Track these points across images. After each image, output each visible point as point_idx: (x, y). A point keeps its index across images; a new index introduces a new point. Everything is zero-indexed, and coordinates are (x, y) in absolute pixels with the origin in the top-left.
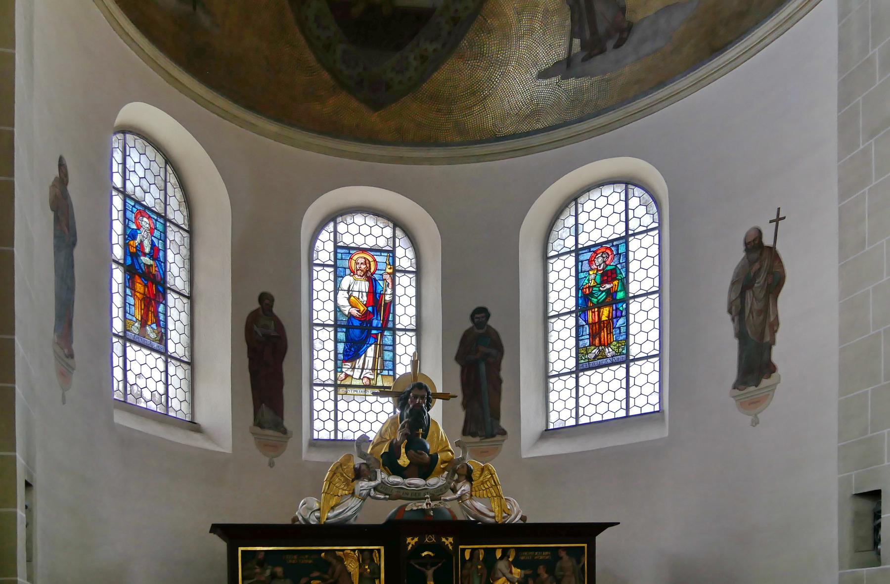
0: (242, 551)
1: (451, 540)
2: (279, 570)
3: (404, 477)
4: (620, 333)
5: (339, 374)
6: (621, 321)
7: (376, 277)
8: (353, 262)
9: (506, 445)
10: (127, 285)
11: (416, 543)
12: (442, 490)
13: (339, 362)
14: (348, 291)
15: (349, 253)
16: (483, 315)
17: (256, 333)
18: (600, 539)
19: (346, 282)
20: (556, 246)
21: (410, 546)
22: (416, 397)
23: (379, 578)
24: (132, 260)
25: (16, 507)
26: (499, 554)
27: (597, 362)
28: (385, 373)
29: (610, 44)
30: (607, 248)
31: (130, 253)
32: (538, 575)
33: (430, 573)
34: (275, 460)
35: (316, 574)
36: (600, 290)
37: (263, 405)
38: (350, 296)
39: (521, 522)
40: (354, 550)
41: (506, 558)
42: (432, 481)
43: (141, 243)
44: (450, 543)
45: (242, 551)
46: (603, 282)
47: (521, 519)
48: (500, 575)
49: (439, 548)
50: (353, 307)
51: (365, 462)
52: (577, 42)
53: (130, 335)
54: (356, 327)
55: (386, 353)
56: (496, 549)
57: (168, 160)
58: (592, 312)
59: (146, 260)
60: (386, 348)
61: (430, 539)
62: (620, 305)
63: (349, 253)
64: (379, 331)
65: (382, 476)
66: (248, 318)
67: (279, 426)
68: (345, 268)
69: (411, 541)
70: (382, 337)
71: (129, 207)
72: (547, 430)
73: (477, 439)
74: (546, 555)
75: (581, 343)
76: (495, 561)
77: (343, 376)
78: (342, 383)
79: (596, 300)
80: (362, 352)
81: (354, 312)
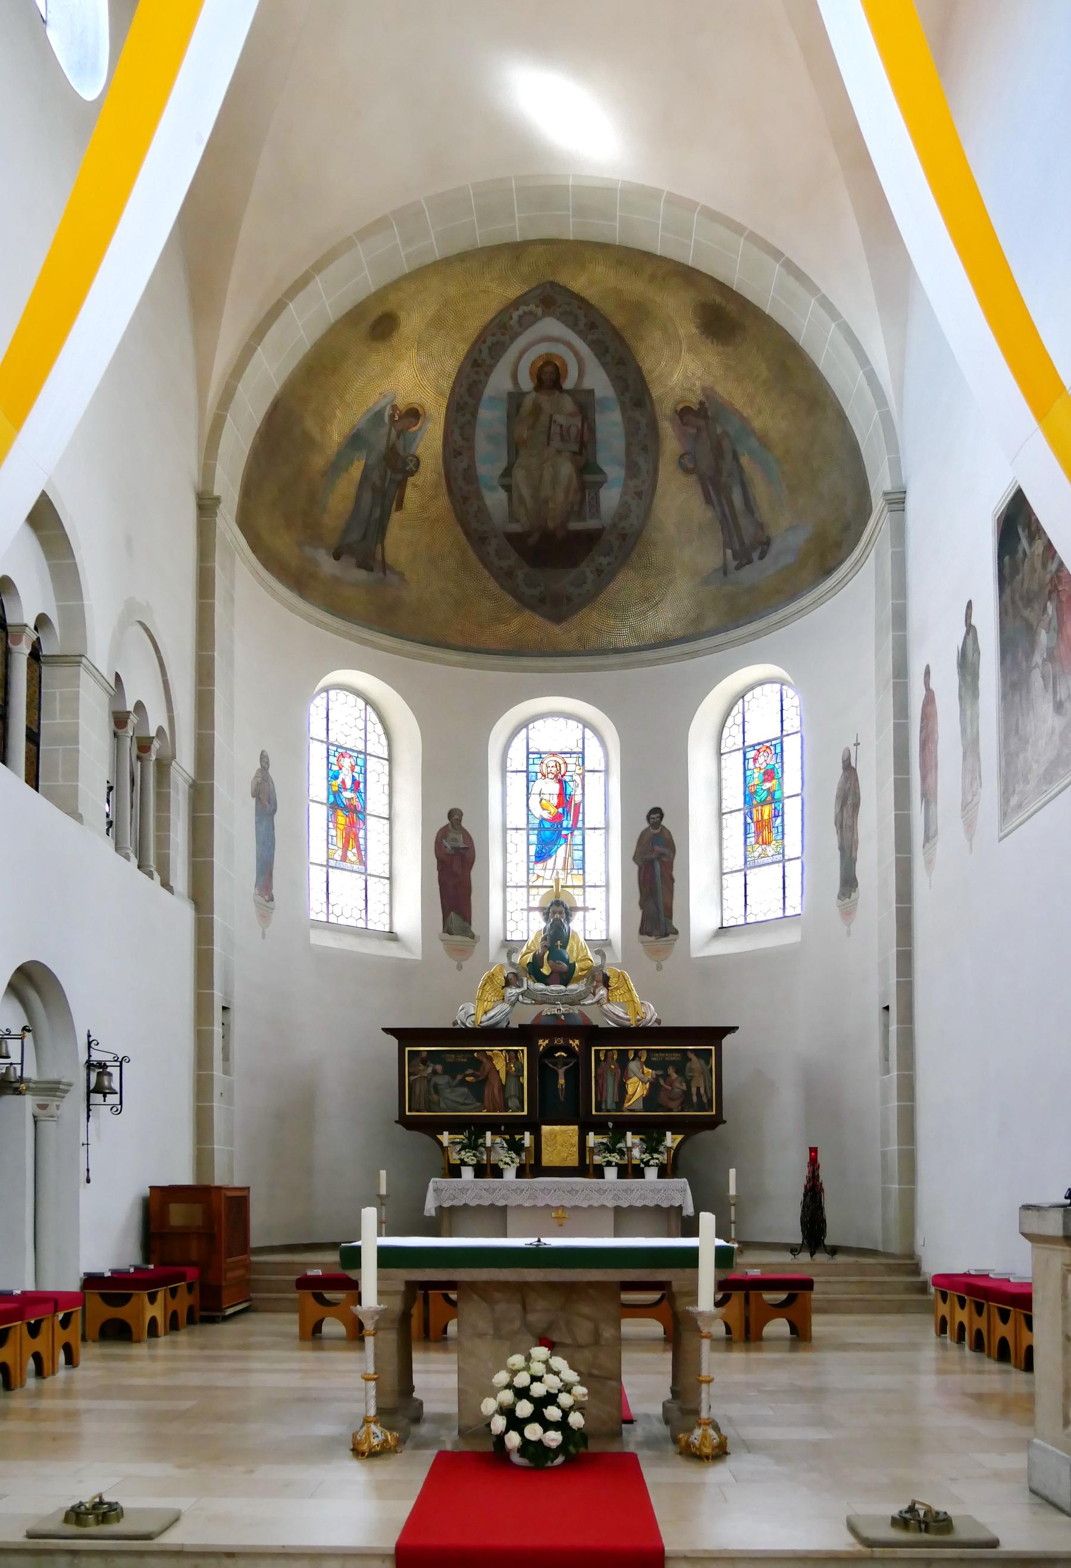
0: (409, 1051)
1: (577, 1042)
2: (439, 1068)
3: (547, 984)
4: (778, 832)
5: (530, 875)
6: (779, 820)
7: (567, 778)
8: (544, 766)
9: (679, 943)
10: (330, 820)
11: (547, 1044)
12: (583, 996)
14: (540, 794)
15: (541, 758)
16: (658, 815)
17: (446, 847)
18: (727, 1041)
19: (536, 788)
20: (728, 744)
21: (542, 1047)
22: (554, 913)
23: (523, 1076)
24: (335, 797)
25: (213, 1025)
28: (575, 872)
29: (755, 555)
30: (767, 747)
31: (333, 791)
32: (669, 1076)
33: (561, 1072)
34: (463, 963)
35: (470, 1071)
36: (762, 789)
38: (541, 800)
39: (656, 1025)
40: (501, 1051)
41: (637, 1058)
42: (571, 987)
43: (343, 782)
45: (409, 1051)
46: (764, 781)
48: (633, 1075)
49: (567, 1049)
50: (544, 809)
51: (514, 971)
52: (729, 552)
53: (332, 863)
54: (547, 829)
55: (576, 853)
57: (368, 702)
58: (757, 810)
59: (348, 794)
60: (576, 847)
61: (559, 1041)
62: (778, 804)
63: (541, 758)
64: (570, 832)
65: (528, 983)
66: (438, 833)
67: (466, 930)
68: (537, 773)
69: (543, 1043)
70: (572, 837)
71: (331, 752)
73: (653, 938)
74: (676, 1057)
75: (748, 840)
76: (628, 1061)
77: (535, 877)
78: (534, 884)
79: (759, 798)
81: (546, 815)
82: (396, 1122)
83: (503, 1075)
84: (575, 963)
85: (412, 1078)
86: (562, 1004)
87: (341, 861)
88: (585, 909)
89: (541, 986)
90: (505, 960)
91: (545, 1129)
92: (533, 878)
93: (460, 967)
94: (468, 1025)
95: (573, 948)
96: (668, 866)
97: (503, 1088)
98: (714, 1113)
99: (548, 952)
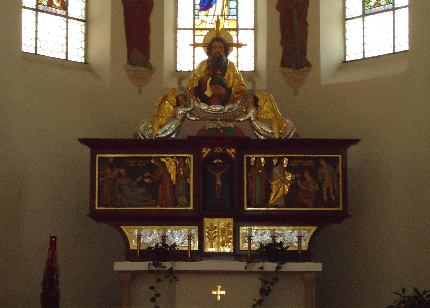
1: (233, 150)
3: (209, 104)
11: (209, 152)
13: (196, 12)
18: (352, 151)
21: (205, 155)
23: (189, 178)
26: (275, 162)
27: (376, 9)
28: (230, 18)
32: (305, 178)
33: (218, 175)
35: (147, 174)
37: (135, 48)
39: (295, 137)
40: (172, 158)
41: (280, 164)
44: (233, 153)
47: (294, 135)
49: (225, 156)
53: (41, 7)
56: (273, 157)
61: (219, 150)
65: (195, 103)
69: (206, 151)
72: (345, 62)
73: (291, 70)
80: (213, 2)
82: (88, 215)
83: (173, 177)
84: (231, 88)
85: (102, 179)
86: (221, 120)
87: (47, 6)
88: (238, 45)
89: (204, 107)
90: (176, 86)
91: (207, 222)
92: (198, 22)
93: (140, 92)
94: (147, 137)
95: (230, 75)
96: (303, 14)
97: (173, 187)
98: (341, 208)
99: (210, 79)
